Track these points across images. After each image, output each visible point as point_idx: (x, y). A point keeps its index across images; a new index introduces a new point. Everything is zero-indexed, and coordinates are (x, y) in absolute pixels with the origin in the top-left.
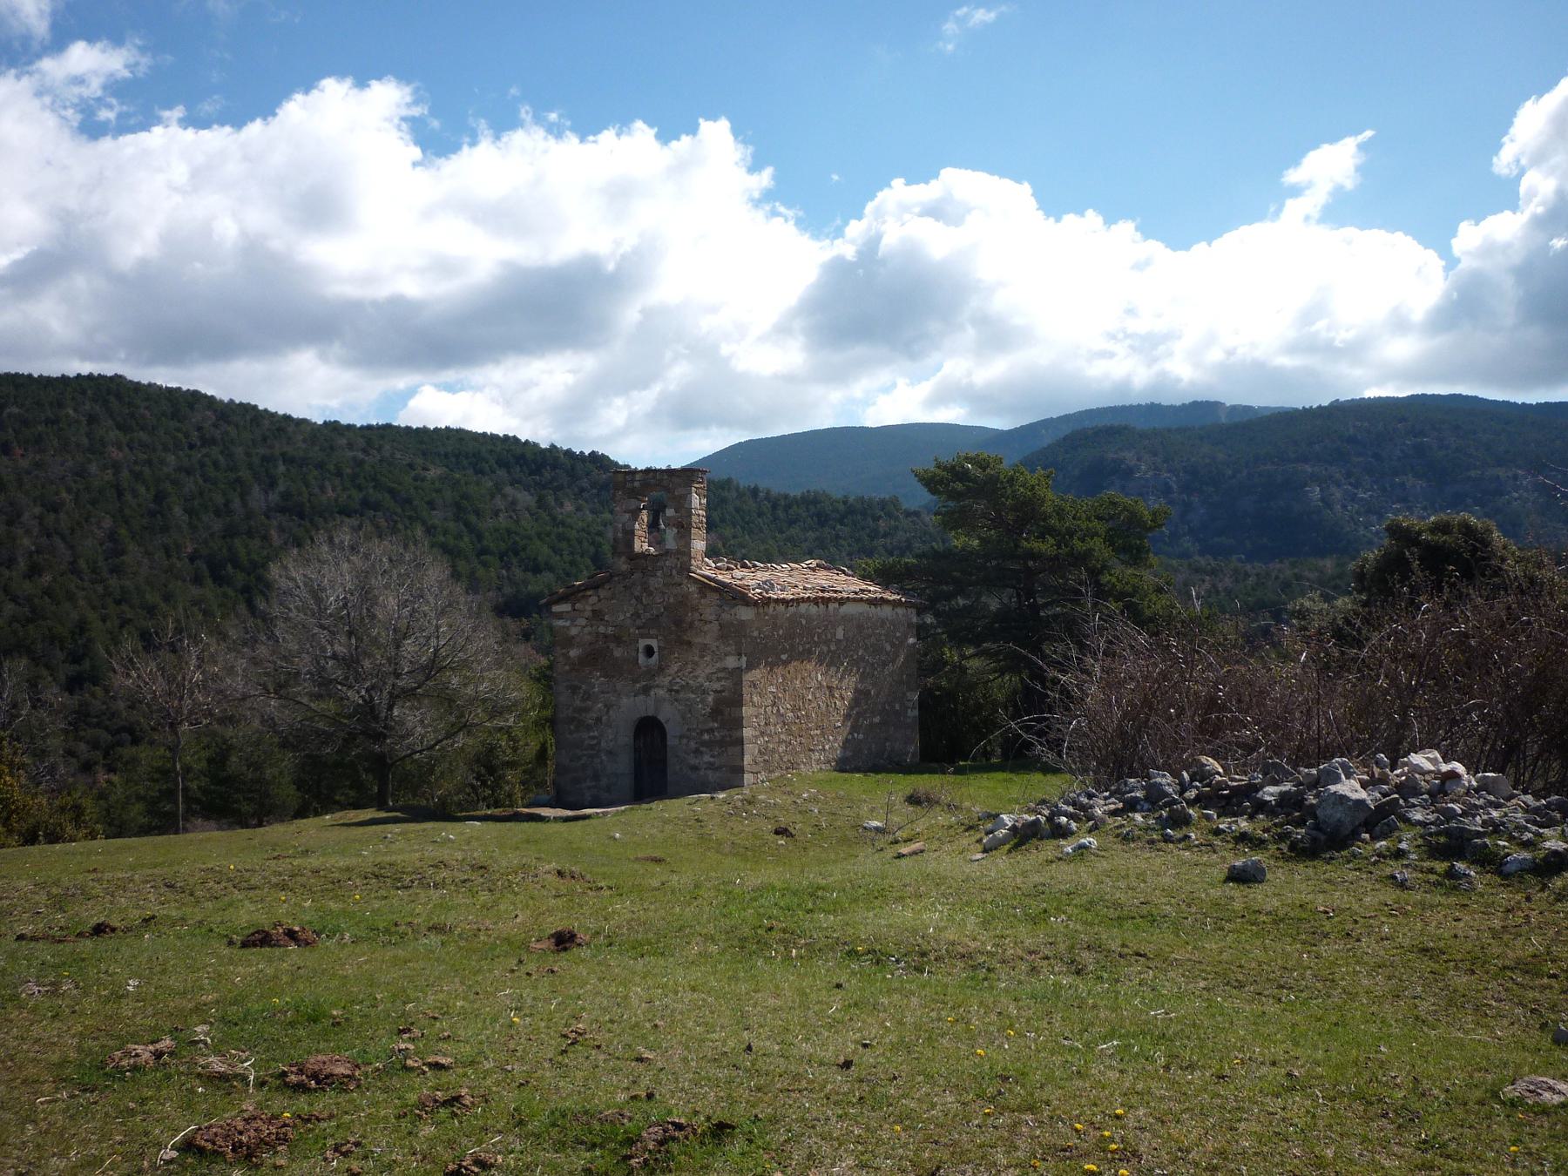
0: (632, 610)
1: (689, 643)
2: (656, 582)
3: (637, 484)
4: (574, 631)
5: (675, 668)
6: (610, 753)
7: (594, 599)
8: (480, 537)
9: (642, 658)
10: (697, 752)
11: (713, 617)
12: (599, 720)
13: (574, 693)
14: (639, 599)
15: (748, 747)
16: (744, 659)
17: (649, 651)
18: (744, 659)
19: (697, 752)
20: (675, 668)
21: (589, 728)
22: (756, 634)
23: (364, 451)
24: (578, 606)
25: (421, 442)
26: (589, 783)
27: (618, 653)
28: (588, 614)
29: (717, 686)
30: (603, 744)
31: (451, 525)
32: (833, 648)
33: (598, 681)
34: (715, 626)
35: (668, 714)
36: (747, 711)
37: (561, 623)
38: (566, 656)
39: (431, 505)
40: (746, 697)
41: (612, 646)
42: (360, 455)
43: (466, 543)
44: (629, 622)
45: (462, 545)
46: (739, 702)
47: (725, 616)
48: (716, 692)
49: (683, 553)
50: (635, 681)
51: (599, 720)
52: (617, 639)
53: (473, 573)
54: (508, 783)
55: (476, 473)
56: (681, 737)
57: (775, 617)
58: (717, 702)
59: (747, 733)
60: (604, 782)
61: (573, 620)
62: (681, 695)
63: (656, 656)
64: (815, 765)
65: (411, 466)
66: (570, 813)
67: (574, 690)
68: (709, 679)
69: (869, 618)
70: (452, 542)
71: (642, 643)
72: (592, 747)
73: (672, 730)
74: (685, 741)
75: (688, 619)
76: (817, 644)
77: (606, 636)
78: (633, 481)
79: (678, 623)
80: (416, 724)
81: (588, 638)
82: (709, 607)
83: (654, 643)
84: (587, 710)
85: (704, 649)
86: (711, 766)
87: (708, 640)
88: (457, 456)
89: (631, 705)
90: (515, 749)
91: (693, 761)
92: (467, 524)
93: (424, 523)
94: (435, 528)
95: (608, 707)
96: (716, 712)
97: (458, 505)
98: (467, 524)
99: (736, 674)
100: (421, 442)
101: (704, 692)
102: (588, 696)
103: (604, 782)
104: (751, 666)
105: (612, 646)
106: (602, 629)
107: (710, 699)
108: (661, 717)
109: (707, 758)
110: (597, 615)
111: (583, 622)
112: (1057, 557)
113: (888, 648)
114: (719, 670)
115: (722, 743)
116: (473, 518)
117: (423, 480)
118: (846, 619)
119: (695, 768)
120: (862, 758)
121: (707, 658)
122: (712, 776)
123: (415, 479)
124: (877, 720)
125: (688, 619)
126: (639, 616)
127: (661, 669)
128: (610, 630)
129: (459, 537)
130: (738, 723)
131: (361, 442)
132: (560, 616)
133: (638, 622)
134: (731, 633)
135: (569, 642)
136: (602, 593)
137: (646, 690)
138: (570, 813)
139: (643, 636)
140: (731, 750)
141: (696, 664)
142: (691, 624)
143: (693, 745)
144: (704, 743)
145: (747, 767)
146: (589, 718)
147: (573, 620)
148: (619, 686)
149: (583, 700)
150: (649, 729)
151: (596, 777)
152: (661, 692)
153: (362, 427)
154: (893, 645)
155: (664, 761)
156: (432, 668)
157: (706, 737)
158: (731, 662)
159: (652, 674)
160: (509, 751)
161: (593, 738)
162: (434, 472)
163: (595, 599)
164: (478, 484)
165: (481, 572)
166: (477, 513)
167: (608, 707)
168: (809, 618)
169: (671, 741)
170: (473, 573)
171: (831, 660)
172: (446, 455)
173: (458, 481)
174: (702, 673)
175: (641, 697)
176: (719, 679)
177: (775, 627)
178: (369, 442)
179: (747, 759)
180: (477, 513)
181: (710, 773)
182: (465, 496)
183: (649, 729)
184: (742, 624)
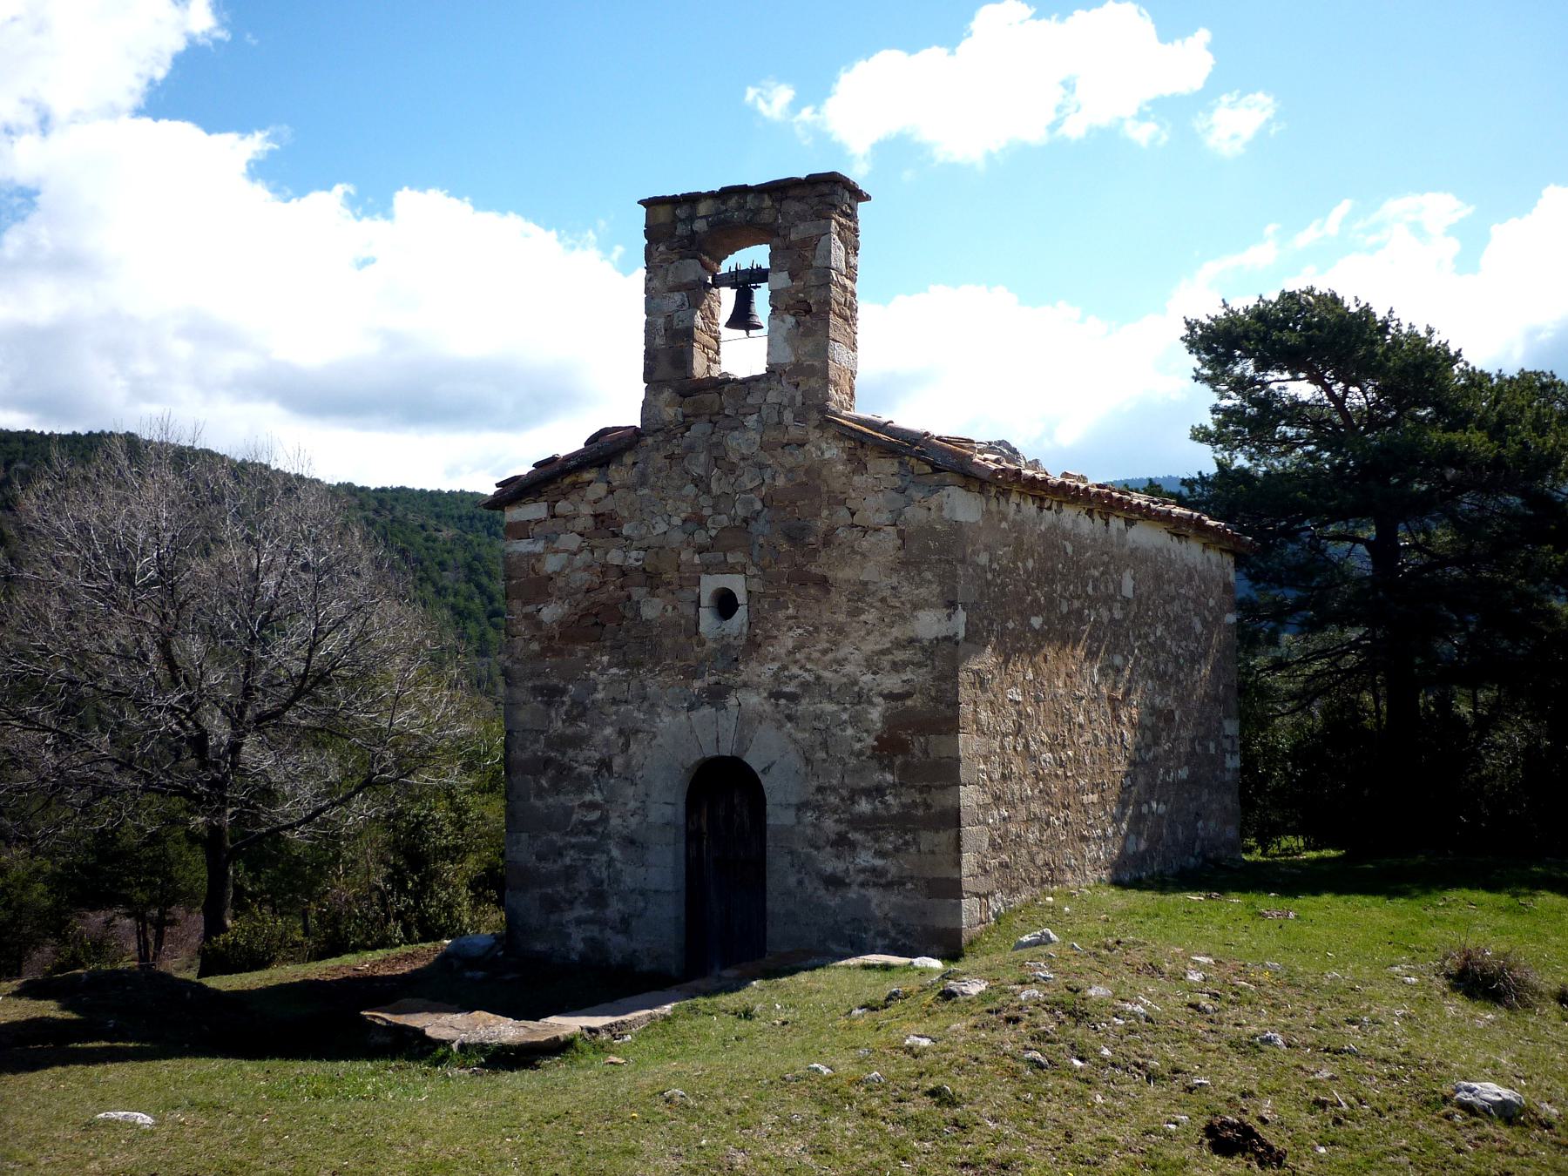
0: (686, 510)
1: (823, 583)
2: (741, 443)
3: (700, 225)
4: (551, 564)
5: (788, 640)
6: (630, 842)
7: (599, 489)
8: (491, 599)
9: (708, 621)
10: (842, 843)
11: (885, 517)
12: (605, 764)
13: (549, 704)
14: (701, 483)
15: (969, 831)
16: (962, 616)
17: (725, 604)
18: (962, 616)
19: (842, 843)
20: (788, 640)
21: (582, 784)
22: (983, 559)
23: (376, 511)
24: (562, 507)
25: (436, 505)
26: (580, 911)
27: (651, 609)
28: (585, 522)
29: (892, 683)
30: (615, 821)
31: (463, 587)
32: (1118, 615)
33: (603, 674)
34: (888, 540)
35: (771, 753)
36: (968, 744)
37: (523, 546)
38: (534, 621)
39: (442, 565)
40: (966, 710)
41: (638, 593)
42: (371, 515)
43: (477, 604)
44: (677, 537)
45: (473, 606)
46: (951, 725)
47: (916, 515)
48: (890, 696)
49: (811, 372)
50: (692, 673)
51: (605, 764)
52: (652, 579)
53: (483, 635)
54: (446, 885)
55: (489, 535)
56: (802, 807)
57: (1018, 527)
58: (893, 722)
59: (969, 796)
60: (615, 908)
61: (550, 539)
62: (804, 706)
63: (741, 615)
64: (1087, 877)
65: (423, 527)
66: (508, 1030)
67: (551, 695)
68: (872, 665)
69: (1170, 562)
70: (461, 603)
71: (709, 585)
72: (589, 828)
73: (780, 793)
74: (809, 816)
75: (821, 525)
76: (1092, 602)
77: (623, 572)
78: (692, 218)
79: (796, 535)
80: (294, 780)
81: (581, 578)
82: (873, 492)
83: (736, 584)
84: (578, 741)
85: (861, 591)
86: (876, 877)
87: (870, 573)
88: (471, 519)
89: (681, 731)
90: (460, 826)
91: (831, 864)
92: (479, 586)
93: (434, 584)
94: (446, 589)
95: (627, 734)
96: (889, 747)
97: (469, 566)
98: (479, 586)
99: (944, 657)
100: (436, 505)
101: (861, 698)
102: (579, 711)
103: (615, 908)
104: (975, 638)
105: (638, 593)
106: (615, 557)
107: (875, 714)
108: (754, 760)
109: (865, 858)
110: (605, 524)
111: (571, 541)
112: (1498, 462)
113: (1198, 628)
114: (899, 645)
115: (904, 822)
116: (485, 580)
117: (435, 540)
118: (1137, 557)
119: (834, 882)
120: (1171, 862)
121: (870, 616)
122: (880, 902)
123: (427, 540)
124: (1183, 773)
125: (821, 525)
126: (701, 522)
127: (753, 645)
128: (634, 558)
129: (470, 598)
130: (947, 773)
131: (374, 504)
132: (520, 531)
133: (701, 537)
134: (931, 553)
135: (541, 588)
136: (617, 474)
137: (717, 695)
138: (508, 1030)
139: (708, 569)
140: (927, 839)
141: (840, 630)
142: (828, 539)
143: (830, 825)
144: (859, 822)
145: (968, 884)
146: (583, 761)
147: (550, 539)
148: (652, 688)
149: (571, 719)
150: (723, 794)
151: (598, 898)
152: (753, 700)
153: (376, 490)
154: (1204, 622)
155: (759, 865)
156: (311, 683)
157: (864, 806)
158: (929, 624)
159: (729, 657)
160: (448, 829)
161: (593, 806)
162: (447, 533)
163: (599, 489)
164: (491, 545)
165: (491, 634)
166: (489, 574)
167: (627, 734)
168: (1076, 539)
169: (778, 817)
170: (483, 635)
171: (1107, 643)
172: (460, 518)
173: (470, 543)
174: (854, 654)
175: (707, 711)
176: (896, 667)
177: (1020, 551)
178: (381, 502)
179: (969, 860)
180: (489, 574)
181: (872, 893)
182: (477, 558)
183: (723, 794)
184: (957, 528)
